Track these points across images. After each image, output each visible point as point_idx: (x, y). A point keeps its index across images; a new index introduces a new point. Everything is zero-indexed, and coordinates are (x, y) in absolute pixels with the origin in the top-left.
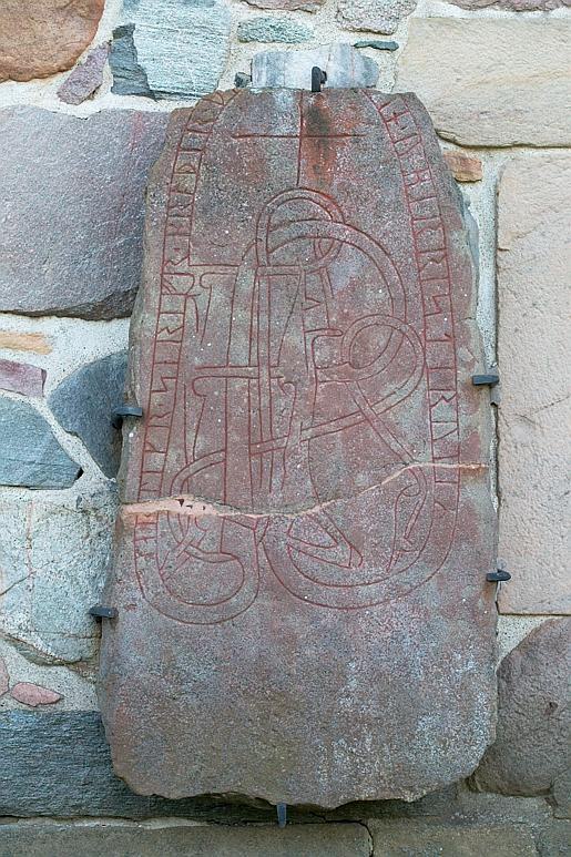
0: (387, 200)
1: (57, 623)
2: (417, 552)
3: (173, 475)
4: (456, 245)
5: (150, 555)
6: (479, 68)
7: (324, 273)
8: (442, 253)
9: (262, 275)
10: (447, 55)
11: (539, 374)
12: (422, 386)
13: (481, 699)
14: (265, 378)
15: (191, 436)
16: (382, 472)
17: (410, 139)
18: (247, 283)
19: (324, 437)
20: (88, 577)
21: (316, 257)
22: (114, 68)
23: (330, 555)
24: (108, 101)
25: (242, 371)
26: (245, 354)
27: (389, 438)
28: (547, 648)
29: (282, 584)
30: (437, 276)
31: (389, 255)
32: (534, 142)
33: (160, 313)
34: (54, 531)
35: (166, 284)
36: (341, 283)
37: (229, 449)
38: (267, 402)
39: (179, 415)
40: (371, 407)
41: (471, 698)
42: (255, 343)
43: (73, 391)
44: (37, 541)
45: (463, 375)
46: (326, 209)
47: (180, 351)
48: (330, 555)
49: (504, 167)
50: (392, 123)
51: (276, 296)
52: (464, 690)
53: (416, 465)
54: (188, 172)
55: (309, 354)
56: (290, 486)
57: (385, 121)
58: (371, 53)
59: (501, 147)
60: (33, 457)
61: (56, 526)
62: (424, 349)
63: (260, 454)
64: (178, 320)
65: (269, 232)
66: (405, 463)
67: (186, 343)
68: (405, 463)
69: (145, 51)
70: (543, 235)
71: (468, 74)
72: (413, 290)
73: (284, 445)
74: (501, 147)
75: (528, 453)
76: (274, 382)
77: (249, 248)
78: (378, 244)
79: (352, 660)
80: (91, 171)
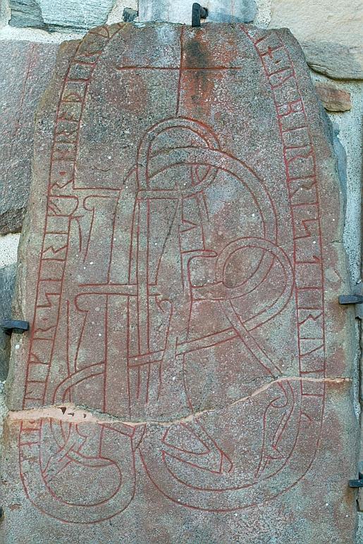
7: (200, 198)
12: (292, 305)
14: (143, 296)
15: (73, 349)
21: (193, 182)
23: (202, 461)
25: (121, 289)
26: (125, 272)
33: (45, 233)
35: (52, 206)
36: (216, 207)
37: (108, 362)
39: (62, 328)
42: (134, 263)
46: (203, 137)
47: (64, 269)
50: (267, 57)
51: (155, 219)
53: (283, 379)
54: (74, 101)
55: (186, 274)
63: (137, 366)
64: (63, 240)
66: (274, 377)
67: (70, 262)
68: (274, 377)
72: (284, 214)
77: (130, 172)
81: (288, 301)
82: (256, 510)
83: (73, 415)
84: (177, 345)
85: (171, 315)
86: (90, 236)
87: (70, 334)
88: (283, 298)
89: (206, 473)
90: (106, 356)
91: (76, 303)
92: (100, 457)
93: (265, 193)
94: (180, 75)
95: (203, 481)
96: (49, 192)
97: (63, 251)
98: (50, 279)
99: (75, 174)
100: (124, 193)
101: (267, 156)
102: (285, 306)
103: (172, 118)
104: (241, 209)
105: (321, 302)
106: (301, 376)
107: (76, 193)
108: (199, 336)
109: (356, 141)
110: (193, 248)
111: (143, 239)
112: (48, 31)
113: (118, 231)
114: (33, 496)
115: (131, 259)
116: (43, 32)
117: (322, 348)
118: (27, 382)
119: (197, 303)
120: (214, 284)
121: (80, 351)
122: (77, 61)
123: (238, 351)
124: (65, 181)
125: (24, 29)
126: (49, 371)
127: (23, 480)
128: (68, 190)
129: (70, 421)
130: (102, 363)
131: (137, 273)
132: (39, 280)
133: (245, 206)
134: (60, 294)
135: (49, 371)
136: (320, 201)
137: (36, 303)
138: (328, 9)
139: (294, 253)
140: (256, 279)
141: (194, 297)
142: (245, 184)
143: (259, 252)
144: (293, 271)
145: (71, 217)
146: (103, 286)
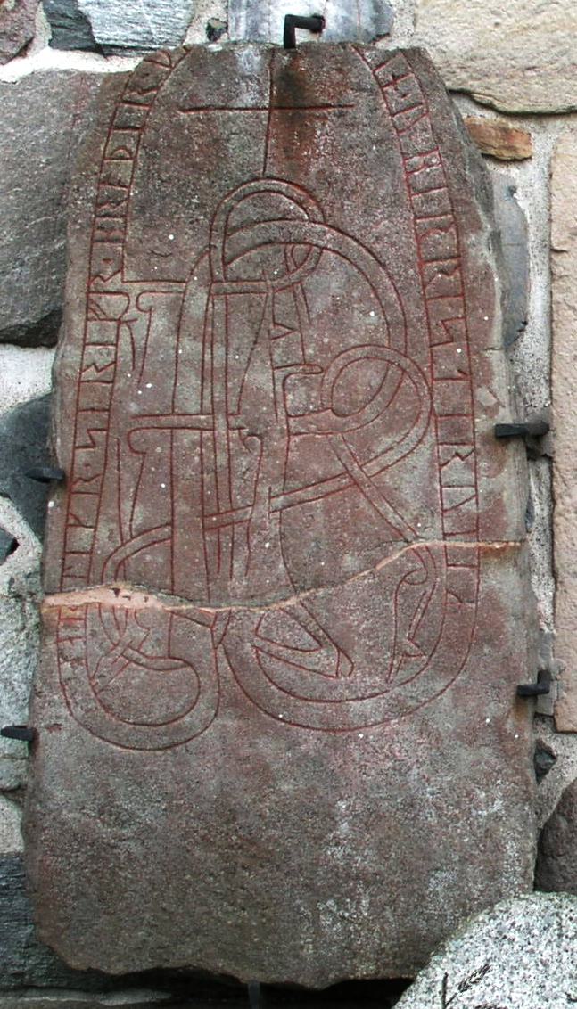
0: (382, 192)
4: (472, 251)
5: (78, 660)
7: (298, 291)
8: (454, 262)
9: (218, 294)
13: (511, 849)
14: (221, 430)
15: (127, 506)
22: (50, 16)
26: (195, 397)
27: (386, 508)
29: (249, 698)
30: (452, 302)
31: (383, 265)
35: (93, 306)
37: (176, 523)
38: (224, 463)
40: (360, 467)
41: (498, 848)
47: (111, 394)
50: (389, 89)
52: (489, 838)
54: (122, 158)
55: (280, 398)
57: (381, 87)
62: (430, 390)
63: (216, 529)
66: (407, 541)
67: (120, 384)
68: (407, 541)
72: (415, 313)
76: (234, 434)
77: (201, 255)
78: (369, 251)
83: (129, 598)
84: (270, 498)
87: (123, 485)
88: (416, 431)
90: (173, 515)
92: (170, 657)
96: (89, 287)
98: (93, 409)
100: (192, 287)
101: (390, 229)
102: (420, 441)
104: (355, 306)
108: (301, 486)
111: (220, 351)
116: (97, 56)
118: (65, 553)
119: (297, 439)
120: (319, 412)
121: (137, 509)
122: (126, 102)
123: (355, 506)
124: (110, 271)
125: (70, 53)
127: (64, 690)
130: (167, 524)
135: (94, 537)
138: (493, 12)
139: (431, 367)
145: (119, 322)
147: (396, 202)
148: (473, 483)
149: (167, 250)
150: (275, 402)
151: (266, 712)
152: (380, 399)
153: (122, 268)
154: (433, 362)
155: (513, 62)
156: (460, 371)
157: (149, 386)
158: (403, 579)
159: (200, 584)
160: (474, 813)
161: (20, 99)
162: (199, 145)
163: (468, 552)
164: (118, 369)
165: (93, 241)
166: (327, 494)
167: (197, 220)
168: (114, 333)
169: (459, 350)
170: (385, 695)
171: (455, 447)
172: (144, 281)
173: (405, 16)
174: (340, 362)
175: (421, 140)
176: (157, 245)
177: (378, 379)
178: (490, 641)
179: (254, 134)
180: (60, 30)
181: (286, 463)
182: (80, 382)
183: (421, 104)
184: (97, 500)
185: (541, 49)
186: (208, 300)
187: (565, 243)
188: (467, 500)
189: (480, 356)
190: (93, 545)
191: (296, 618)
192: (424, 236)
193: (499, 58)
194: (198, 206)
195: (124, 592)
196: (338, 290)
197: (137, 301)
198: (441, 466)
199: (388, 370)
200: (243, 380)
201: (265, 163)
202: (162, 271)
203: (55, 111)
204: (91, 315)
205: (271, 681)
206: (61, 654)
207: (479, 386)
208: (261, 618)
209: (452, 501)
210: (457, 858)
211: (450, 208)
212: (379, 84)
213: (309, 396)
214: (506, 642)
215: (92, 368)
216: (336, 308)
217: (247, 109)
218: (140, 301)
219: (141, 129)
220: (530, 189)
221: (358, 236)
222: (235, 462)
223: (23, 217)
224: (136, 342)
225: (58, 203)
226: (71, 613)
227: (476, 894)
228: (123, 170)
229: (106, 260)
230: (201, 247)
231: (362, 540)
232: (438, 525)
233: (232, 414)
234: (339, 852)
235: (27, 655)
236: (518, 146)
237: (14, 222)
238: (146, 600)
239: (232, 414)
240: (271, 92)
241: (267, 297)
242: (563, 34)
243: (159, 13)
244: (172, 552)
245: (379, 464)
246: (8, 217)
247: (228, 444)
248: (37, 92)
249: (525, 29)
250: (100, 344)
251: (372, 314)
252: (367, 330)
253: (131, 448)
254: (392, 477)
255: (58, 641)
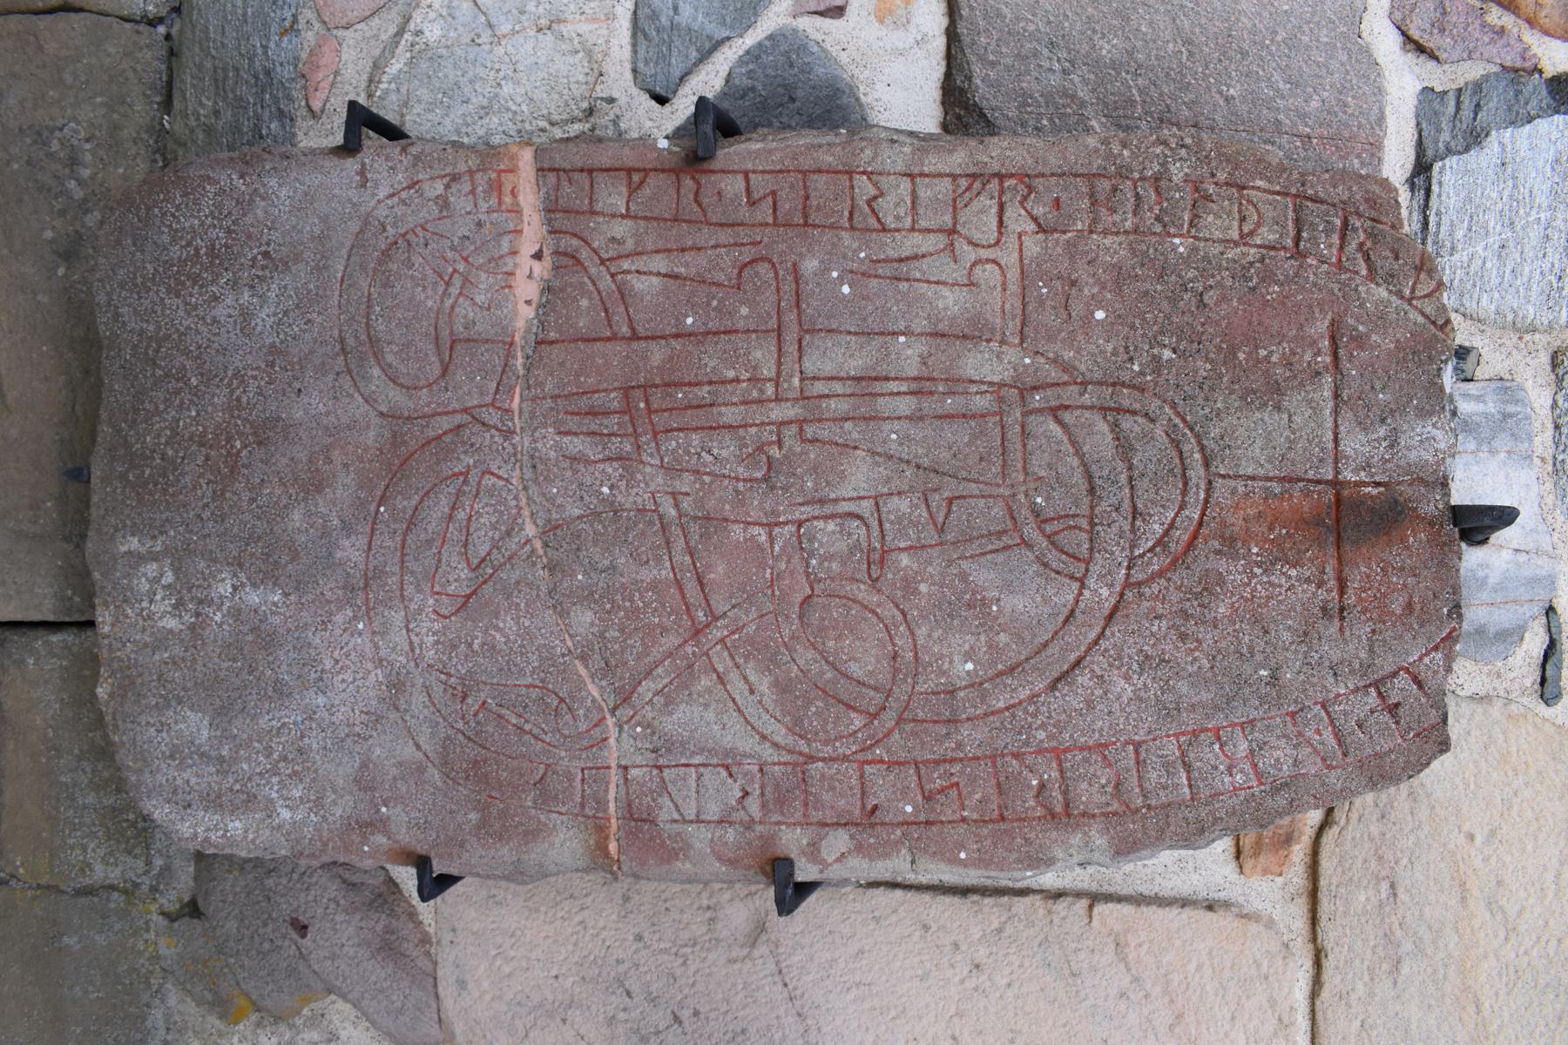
0: (1183, 687)
1: (423, 93)
2: (460, 725)
3: (585, 234)
4: (1076, 840)
6: (1499, 883)
7: (1006, 538)
8: (1059, 809)
9: (1001, 400)
10: (1529, 814)
11: (842, 965)
12: (768, 753)
13: (236, 826)
14: (778, 413)
15: (660, 263)
16: (597, 662)
17: (1332, 741)
18: (982, 364)
19: (659, 541)
20: (489, 134)
21: (1046, 521)
22: (1478, 87)
23: (451, 556)
24: (1403, 82)
25: (790, 362)
26: (828, 368)
28: (388, 930)
29: (410, 459)
30: (991, 811)
31: (1053, 687)
32: (1325, 994)
33: (911, 176)
34: (561, 65)
35: (977, 185)
36: (984, 576)
37: (635, 345)
38: (726, 420)
39: (705, 236)
40: (722, 640)
42: (849, 388)
43: (807, 70)
44: (548, 39)
45: (792, 841)
46: (1159, 542)
47: (832, 227)
48: (451, 556)
49: (1270, 924)
50: (1372, 698)
51: (956, 435)
52: (249, 801)
53: (613, 733)
54: (1243, 219)
55: (828, 509)
56: (569, 473)
57: (1376, 684)
58: (1535, 642)
59: (1314, 921)
60: (686, 11)
61: (573, 70)
62: (845, 758)
63: (627, 409)
64: (897, 218)
65: (1104, 409)
66: (615, 708)
67: (847, 238)
68: (615, 708)
69: (1522, 144)
70: (1122, 995)
71: (1486, 860)
72: (971, 737)
73: (645, 458)
74: (1314, 921)
75: (698, 930)
76: (769, 435)
77: (1067, 368)
78: (1078, 663)
79: (286, 595)
80: (1244, 54)
81: (776, 745)
82: (370, 666)
83: (530, 277)
84: (673, 494)
85: (737, 479)
86: (907, 280)
87: (688, 256)
88: (780, 734)
89: (430, 562)
90: (647, 338)
91: (753, 261)
92: (454, 342)
93: (1024, 693)
94: (1319, 482)
95: (416, 559)
96: (1012, 176)
97: (873, 222)
98: (807, 198)
99: (1056, 235)
100: (1011, 354)
101: (1114, 700)
102: (764, 737)
103: (1207, 464)
104: (983, 638)
105: (776, 817)
106: (619, 766)
107: (1011, 242)
108: (692, 543)
109: (1170, 885)
110: (887, 526)
111: (905, 405)
112: (1413, 176)
113: (921, 347)
114: (382, 212)
115: (858, 379)
116: (1409, 167)
117: (676, 816)
118: (591, 171)
119: (763, 538)
120: (808, 575)
121: (655, 280)
122: (1345, 223)
123: (665, 630)
124: (1039, 210)
125: (1413, 123)
126: (613, 216)
127: (409, 187)
128: (1017, 220)
129: (518, 272)
130: (633, 330)
131: (828, 396)
132: (804, 173)
133: (990, 647)
134: (775, 224)
135: (613, 216)
136: (1003, 826)
137: (754, 172)
138: (1493, 833)
139: (882, 762)
140: (822, 673)
141: (777, 530)
142: (1045, 645)
143: (884, 678)
144: (845, 758)
145: (952, 232)
146: (796, 323)
147: (1168, 712)
148: (702, 817)
149: (1077, 308)
150: (822, 502)
151: (387, 487)
152: (829, 675)
153: (1044, 231)
154: (890, 765)
155: (1405, 861)
156: (875, 808)
157: (846, 289)
158: (562, 700)
159: (549, 386)
160: (275, 780)
161: (1335, 46)
162: (1267, 358)
163: (602, 804)
164: (874, 235)
165: (1091, 177)
166: (680, 588)
167: (1131, 359)
168: (932, 225)
169: (909, 809)
170: (412, 664)
171: (758, 792)
172: (1022, 272)
173: (1487, 680)
174: (889, 611)
175: (1280, 756)
176: (1086, 291)
177: (861, 673)
178: (483, 824)
179: (1291, 455)
180: (1452, 103)
181: (726, 520)
182: (850, 173)
183: (1345, 755)
184: (667, 216)
185: (1427, 910)
186: (991, 384)
187: (1104, 924)
188: (676, 806)
189: (899, 842)
190: (602, 214)
191: (509, 533)
192: (1105, 757)
193: (1412, 839)
194: (1157, 359)
195: (538, 268)
196: (1008, 609)
197: (988, 261)
198: (727, 768)
199: (875, 689)
200: (855, 448)
201: (1237, 477)
202: (1041, 302)
203: (1314, 104)
204: (964, 183)
205: (427, 494)
206: (455, 178)
207: (852, 837)
208: (507, 480)
209: (674, 783)
210: (224, 753)
211: (1153, 803)
212: (1383, 680)
213: (830, 557)
214: (483, 846)
215: (873, 191)
216: (978, 604)
217: (1336, 440)
218: (988, 266)
219: (1299, 254)
220: (1190, 866)
221: (1104, 644)
222: (727, 436)
223: (1140, 66)
224: (916, 263)
225: (1164, 119)
226: (507, 188)
227: (186, 776)
228: (1219, 224)
229: (1057, 203)
230: (1083, 368)
231: (615, 640)
232: (639, 760)
233: (801, 429)
234: (225, 588)
235: (519, 131)
236: (1262, 859)
237: (1130, 54)
238: (528, 302)
239: (801, 429)
240: (1366, 484)
241: (998, 486)
242: (1451, 946)
243: (1489, 265)
244: (595, 340)
245: (727, 671)
246: (1139, 44)
247: (754, 425)
248: (1347, 72)
249: (1463, 884)
250: (913, 203)
251: (969, 666)
252: (942, 657)
253: (745, 265)
254: (709, 690)
255: (471, 172)
